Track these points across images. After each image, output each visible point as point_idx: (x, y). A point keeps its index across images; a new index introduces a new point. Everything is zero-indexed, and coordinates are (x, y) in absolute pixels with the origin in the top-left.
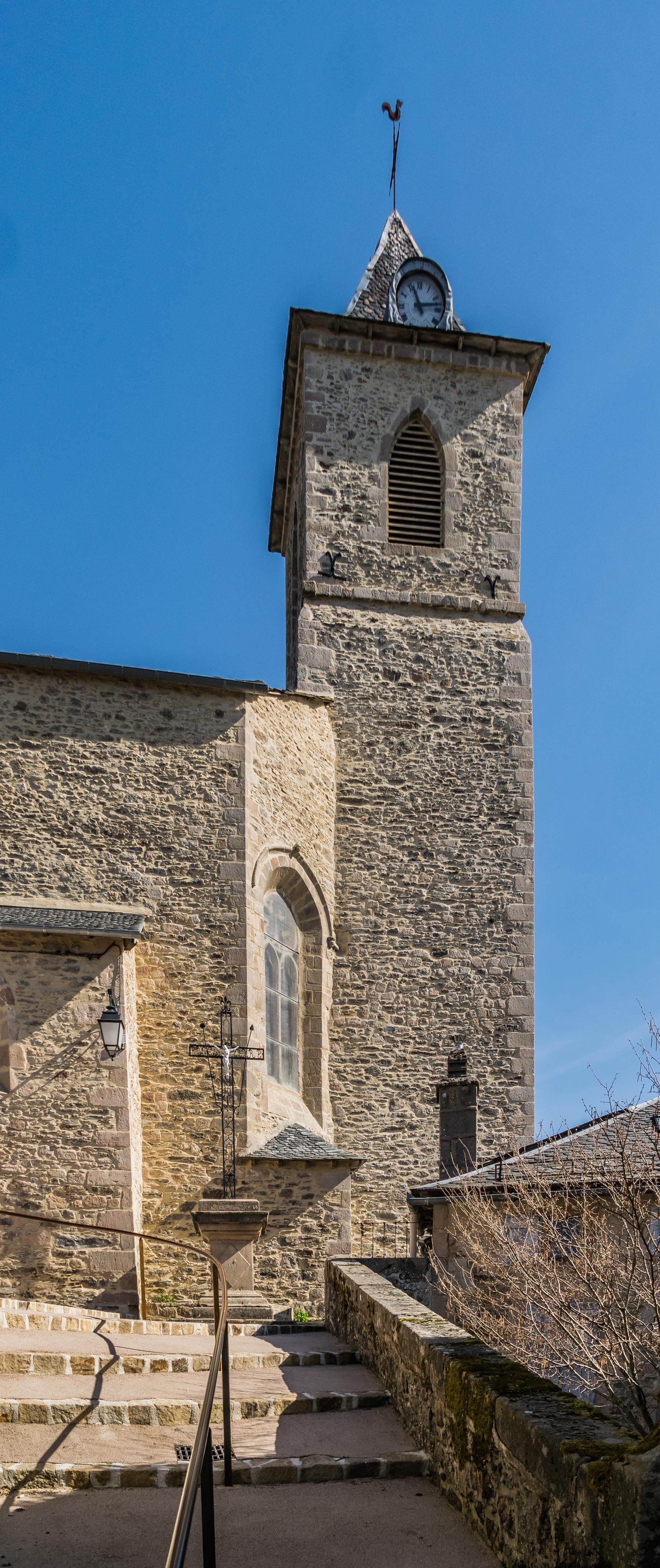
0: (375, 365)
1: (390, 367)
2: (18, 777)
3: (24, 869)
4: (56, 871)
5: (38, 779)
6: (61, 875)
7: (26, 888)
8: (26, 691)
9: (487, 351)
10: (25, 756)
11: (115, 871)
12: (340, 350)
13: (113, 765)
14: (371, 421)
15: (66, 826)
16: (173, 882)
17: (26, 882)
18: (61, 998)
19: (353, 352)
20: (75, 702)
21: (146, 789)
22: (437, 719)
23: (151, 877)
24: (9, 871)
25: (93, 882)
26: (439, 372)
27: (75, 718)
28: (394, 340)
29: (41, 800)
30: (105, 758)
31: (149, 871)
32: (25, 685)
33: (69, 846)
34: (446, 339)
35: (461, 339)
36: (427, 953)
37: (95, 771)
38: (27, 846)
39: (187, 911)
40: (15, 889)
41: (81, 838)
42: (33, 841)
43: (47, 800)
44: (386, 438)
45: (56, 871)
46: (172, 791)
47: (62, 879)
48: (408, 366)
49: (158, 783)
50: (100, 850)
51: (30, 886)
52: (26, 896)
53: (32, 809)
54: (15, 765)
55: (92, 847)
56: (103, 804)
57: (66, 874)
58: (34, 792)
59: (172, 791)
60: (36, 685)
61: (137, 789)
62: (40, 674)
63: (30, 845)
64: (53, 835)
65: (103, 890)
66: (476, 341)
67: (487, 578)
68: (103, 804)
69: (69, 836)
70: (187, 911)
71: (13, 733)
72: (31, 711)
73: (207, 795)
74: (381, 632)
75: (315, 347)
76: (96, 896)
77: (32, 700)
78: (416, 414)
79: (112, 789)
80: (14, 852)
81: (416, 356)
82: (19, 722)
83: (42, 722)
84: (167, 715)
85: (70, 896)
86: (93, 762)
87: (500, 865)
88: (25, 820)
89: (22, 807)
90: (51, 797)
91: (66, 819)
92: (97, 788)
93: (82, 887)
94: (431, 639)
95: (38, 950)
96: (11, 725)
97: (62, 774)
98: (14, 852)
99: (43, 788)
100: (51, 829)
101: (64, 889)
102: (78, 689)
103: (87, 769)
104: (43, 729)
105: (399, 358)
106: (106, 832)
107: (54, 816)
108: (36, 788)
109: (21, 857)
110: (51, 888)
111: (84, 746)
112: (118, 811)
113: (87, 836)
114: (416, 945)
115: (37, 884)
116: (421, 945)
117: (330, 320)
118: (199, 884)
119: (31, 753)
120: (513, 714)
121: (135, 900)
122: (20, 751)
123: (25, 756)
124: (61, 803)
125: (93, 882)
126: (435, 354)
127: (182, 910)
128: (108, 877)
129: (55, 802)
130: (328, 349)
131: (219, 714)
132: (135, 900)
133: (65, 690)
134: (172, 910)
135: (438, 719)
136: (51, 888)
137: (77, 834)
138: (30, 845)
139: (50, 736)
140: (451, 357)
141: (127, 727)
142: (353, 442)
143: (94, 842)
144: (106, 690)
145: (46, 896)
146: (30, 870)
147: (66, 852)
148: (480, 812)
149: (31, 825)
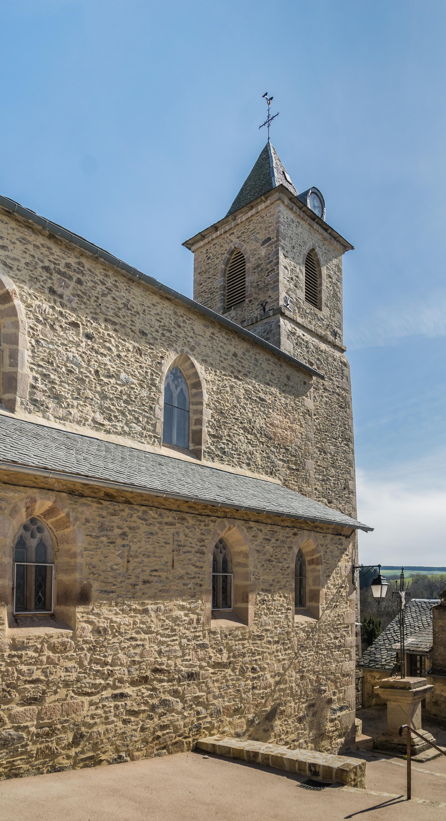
0: (302, 222)
1: (306, 226)
2: (232, 394)
3: (233, 450)
4: (246, 453)
5: (240, 398)
6: (248, 456)
7: (233, 462)
8: (237, 347)
9: (335, 238)
10: (236, 383)
11: (269, 458)
12: (291, 209)
13: (270, 399)
14: (300, 245)
15: (250, 428)
16: (289, 468)
17: (233, 458)
18: (337, 560)
19: (295, 212)
20: (256, 360)
21: (280, 415)
22: (325, 389)
23: (281, 463)
24: (226, 450)
25: (260, 463)
26: (320, 237)
27: (256, 368)
28: (308, 216)
29: (241, 410)
30: (266, 394)
31: (280, 460)
32: (237, 344)
33: (251, 440)
34: (325, 226)
35: (331, 230)
36: (325, 501)
37: (262, 400)
38: (234, 436)
39: (294, 484)
40: (228, 461)
41: (256, 436)
42: (237, 434)
43: (244, 411)
44: (304, 254)
45: (246, 453)
46: (289, 419)
47: (248, 459)
48: (311, 229)
49: (285, 413)
50: (263, 445)
51: (234, 460)
52: (233, 466)
53: (237, 415)
54: (232, 387)
55: (260, 442)
56: (265, 419)
57: (250, 456)
58: (238, 405)
59: (289, 419)
60: (242, 345)
61: (278, 414)
62: (243, 340)
63: (236, 436)
64: (245, 432)
65: (264, 468)
66: (334, 233)
67: (334, 331)
68: (265, 419)
69: (251, 434)
70: (294, 484)
71: (231, 369)
72: (239, 359)
73: (301, 424)
74: (307, 342)
75: (283, 202)
76: (261, 470)
77: (240, 353)
78: (313, 250)
79: (269, 412)
80: (228, 438)
81: (315, 227)
82: (234, 363)
83: (244, 367)
84: (288, 378)
85: (250, 469)
86: (261, 395)
87: (346, 462)
88: (234, 420)
89: (233, 413)
90: (245, 410)
91: (250, 424)
92: (263, 409)
93: (256, 465)
94: (322, 351)
95: (331, 532)
96: (231, 364)
97: (250, 398)
98: (228, 438)
99: (242, 404)
100: (244, 429)
101: (248, 465)
102: (258, 353)
103: (260, 398)
104: (244, 371)
105: (309, 224)
106: (265, 435)
107: (246, 421)
108: (239, 403)
109: (232, 443)
110: (243, 463)
111: (259, 385)
112: (270, 424)
113: (258, 435)
114: (323, 497)
115: (238, 460)
116: (324, 497)
117: (291, 196)
118: (298, 470)
119: (239, 383)
120: (347, 395)
121: (275, 476)
122: (234, 380)
123: (236, 383)
124: (249, 414)
125: (260, 463)
126: (321, 230)
127: (292, 484)
128: (266, 460)
129: (247, 413)
130: (287, 206)
131: (305, 383)
132: (275, 476)
133: (253, 351)
134: (289, 483)
135: (325, 389)
136: (243, 463)
137: (254, 433)
138: (236, 436)
139: (246, 375)
140: (325, 234)
141: (275, 380)
142: (294, 251)
143: (261, 440)
144: (267, 358)
145: (241, 467)
146: (235, 451)
147: (250, 443)
148: (339, 436)
149: (236, 424)
